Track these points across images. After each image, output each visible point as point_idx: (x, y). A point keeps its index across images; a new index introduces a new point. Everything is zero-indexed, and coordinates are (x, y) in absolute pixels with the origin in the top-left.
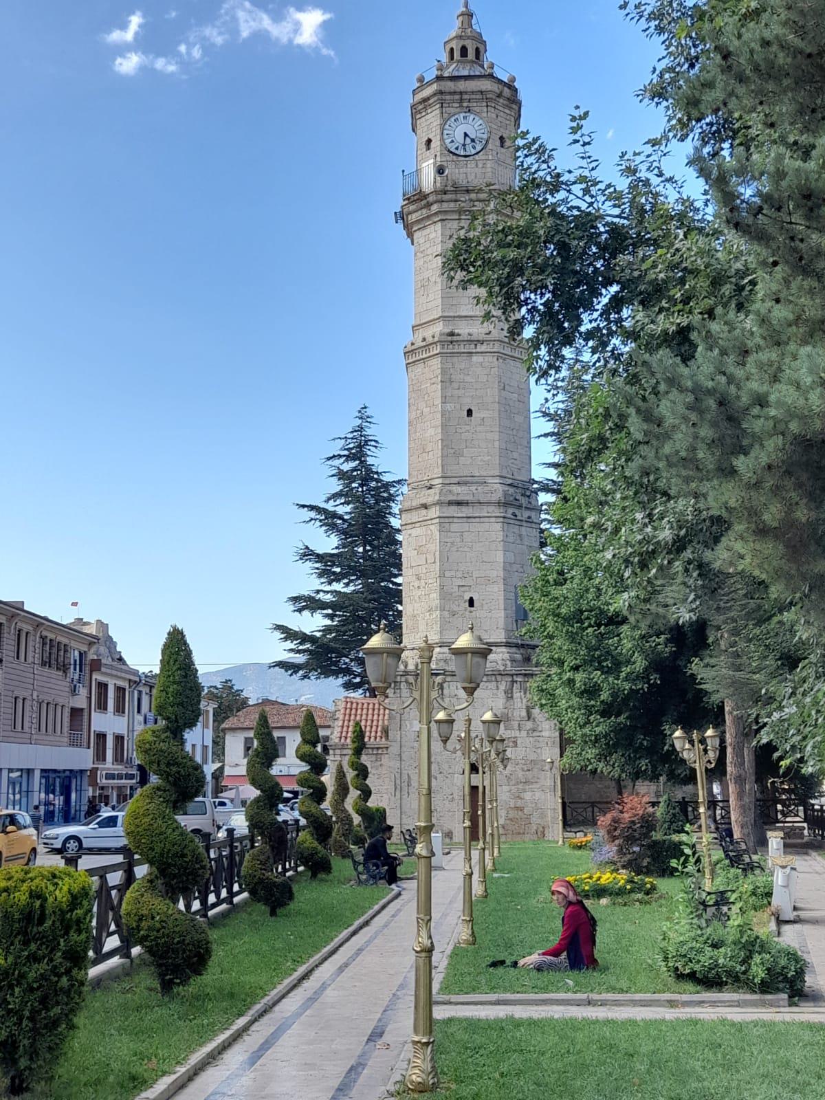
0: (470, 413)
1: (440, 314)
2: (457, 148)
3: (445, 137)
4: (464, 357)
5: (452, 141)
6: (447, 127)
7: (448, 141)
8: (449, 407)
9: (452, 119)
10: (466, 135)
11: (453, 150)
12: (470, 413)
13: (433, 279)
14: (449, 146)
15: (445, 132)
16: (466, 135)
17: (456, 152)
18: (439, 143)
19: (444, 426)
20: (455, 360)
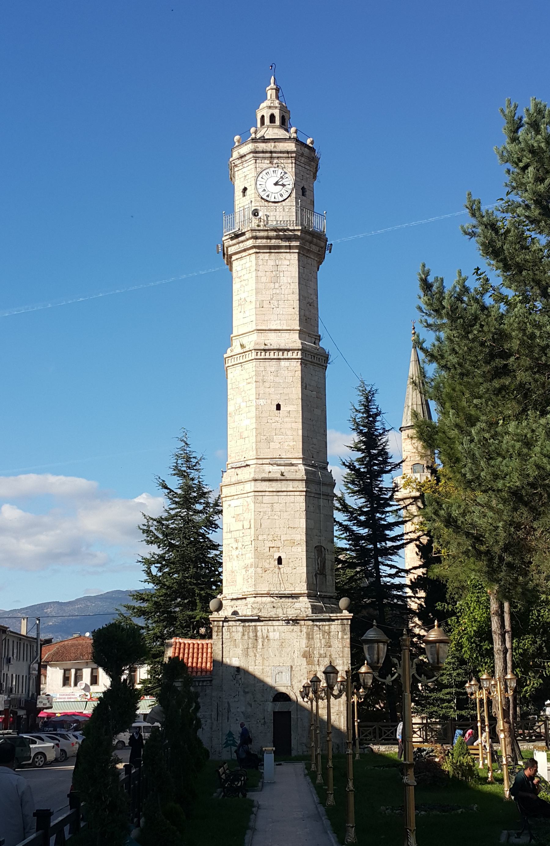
0: (278, 407)
1: (254, 328)
2: (268, 196)
3: (258, 186)
4: (274, 362)
5: (264, 190)
6: (259, 178)
7: (260, 191)
8: (262, 402)
9: (264, 173)
10: (276, 184)
11: (265, 197)
12: (278, 407)
13: (248, 300)
14: (262, 194)
15: (258, 183)
16: (276, 184)
17: (267, 199)
18: (253, 191)
19: (258, 418)
20: (267, 364)
